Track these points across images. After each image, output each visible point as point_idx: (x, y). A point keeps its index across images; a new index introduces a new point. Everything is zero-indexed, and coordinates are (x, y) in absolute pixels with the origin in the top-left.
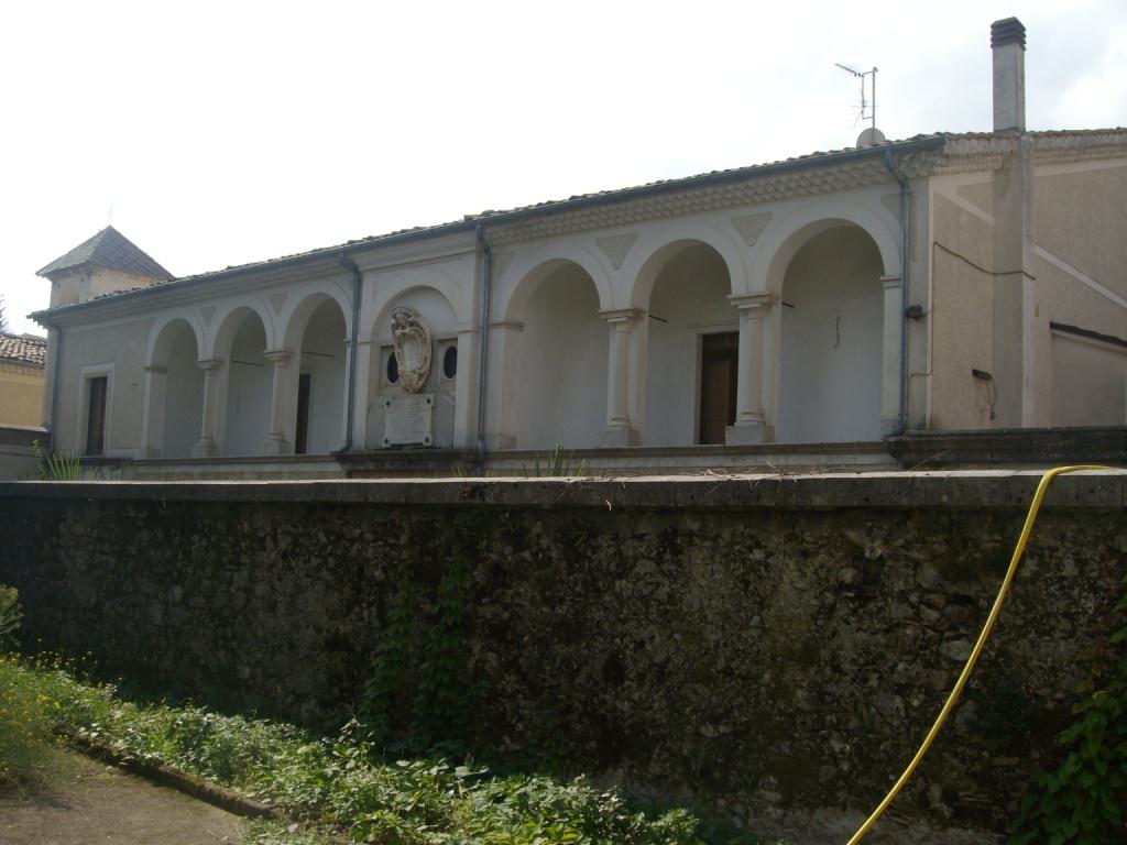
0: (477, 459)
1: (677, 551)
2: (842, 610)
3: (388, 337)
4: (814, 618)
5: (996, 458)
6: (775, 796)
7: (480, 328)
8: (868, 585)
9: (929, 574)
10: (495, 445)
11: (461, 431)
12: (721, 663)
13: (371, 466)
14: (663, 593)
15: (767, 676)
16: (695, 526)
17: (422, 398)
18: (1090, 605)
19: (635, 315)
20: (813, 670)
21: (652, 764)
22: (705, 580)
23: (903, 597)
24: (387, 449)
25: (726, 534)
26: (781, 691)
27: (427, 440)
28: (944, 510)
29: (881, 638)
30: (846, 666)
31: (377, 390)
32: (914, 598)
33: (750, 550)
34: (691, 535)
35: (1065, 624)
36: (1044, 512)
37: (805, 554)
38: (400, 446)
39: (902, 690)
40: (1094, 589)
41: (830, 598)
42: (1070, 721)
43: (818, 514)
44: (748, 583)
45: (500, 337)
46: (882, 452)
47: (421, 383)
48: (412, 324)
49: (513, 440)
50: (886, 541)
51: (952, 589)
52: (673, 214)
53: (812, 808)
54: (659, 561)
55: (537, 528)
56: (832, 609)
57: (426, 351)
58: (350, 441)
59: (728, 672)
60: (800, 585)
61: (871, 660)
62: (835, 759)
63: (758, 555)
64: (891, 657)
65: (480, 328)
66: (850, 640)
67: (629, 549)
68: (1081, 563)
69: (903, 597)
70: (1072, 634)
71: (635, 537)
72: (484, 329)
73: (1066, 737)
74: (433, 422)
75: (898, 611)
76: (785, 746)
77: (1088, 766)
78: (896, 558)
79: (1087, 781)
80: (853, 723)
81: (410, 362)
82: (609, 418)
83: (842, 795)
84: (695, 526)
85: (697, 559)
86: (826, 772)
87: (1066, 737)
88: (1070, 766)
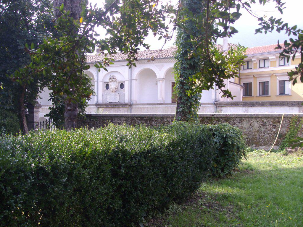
0: (130, 105)
1: (242, 122)
2: (262, 127)
3: (107, 80)
4: (259, 128)
5: (232, 105)
6: (255, 146)
7: (129, 80)
8: (264, 124)
9: (271, 123)
10: (134, 102)
11: (126, 100)
12: (248, 133)
13: (105, 106)
14: (240, 126)
15: (253, 134)
16: (244, 119)
17: (117, 93)
18: (287, 125)
19: (163, 79)
20: (259, 133)
21: (50, 190)
22: (245, 124)
23: (268, 125)
24: (108, 103)
25: (248, 120)
26: (255, 135)
27: (118, 101)
28: (273, 117)
29: (266, 129)
30: (262, 132)
31: (104, 91)
32: (269, 125)
33: (251, 121)
34: (243, 120)
35: (284, 127)
36: (284, 117)
37: (258, 121)
38: (111, 103)
39: (268, 134)
40: (287, 124)
41: (260, 126)
42: (285, 135)
43: (259, 117)
44: (251, 125)
45: (134, 82)
46: (213, 104)
47: (116, 90)
48: (114, 79)
49: (136, 102)
50: (267, 120)
51: (273, 124)
52: (172, 62)
53: (259, 146)
54: (239, 122)
55: (221, 119)
56: (261, 127)
57: (117, 84)
58: (97, 102)
59: (248, 134)
60: (257, 124)
61: (265, 131)
62: (261, 141)
63: (252, 122)
64: (267, 131)
65: (129, 80)
66: (263, 129)
67: (235, 121)
68: (286, 122)
69: (268, 125)
70: (285, 128)
71: (236, 120)
72: (131, 80)
73: (285, 137)
74: (119, 98)
75: (268, 127)
76: (256, 141)
77: (287, 139)
78: (267, 121)
79: (288, 140)
80: (263, 138)
81: (113, 86)
82: (158, 98)
83: (262, 145)
84: (244, 119)
85: (244, 122)
86: (260, 143)
87: (285, 137)
88: (286, 139)
